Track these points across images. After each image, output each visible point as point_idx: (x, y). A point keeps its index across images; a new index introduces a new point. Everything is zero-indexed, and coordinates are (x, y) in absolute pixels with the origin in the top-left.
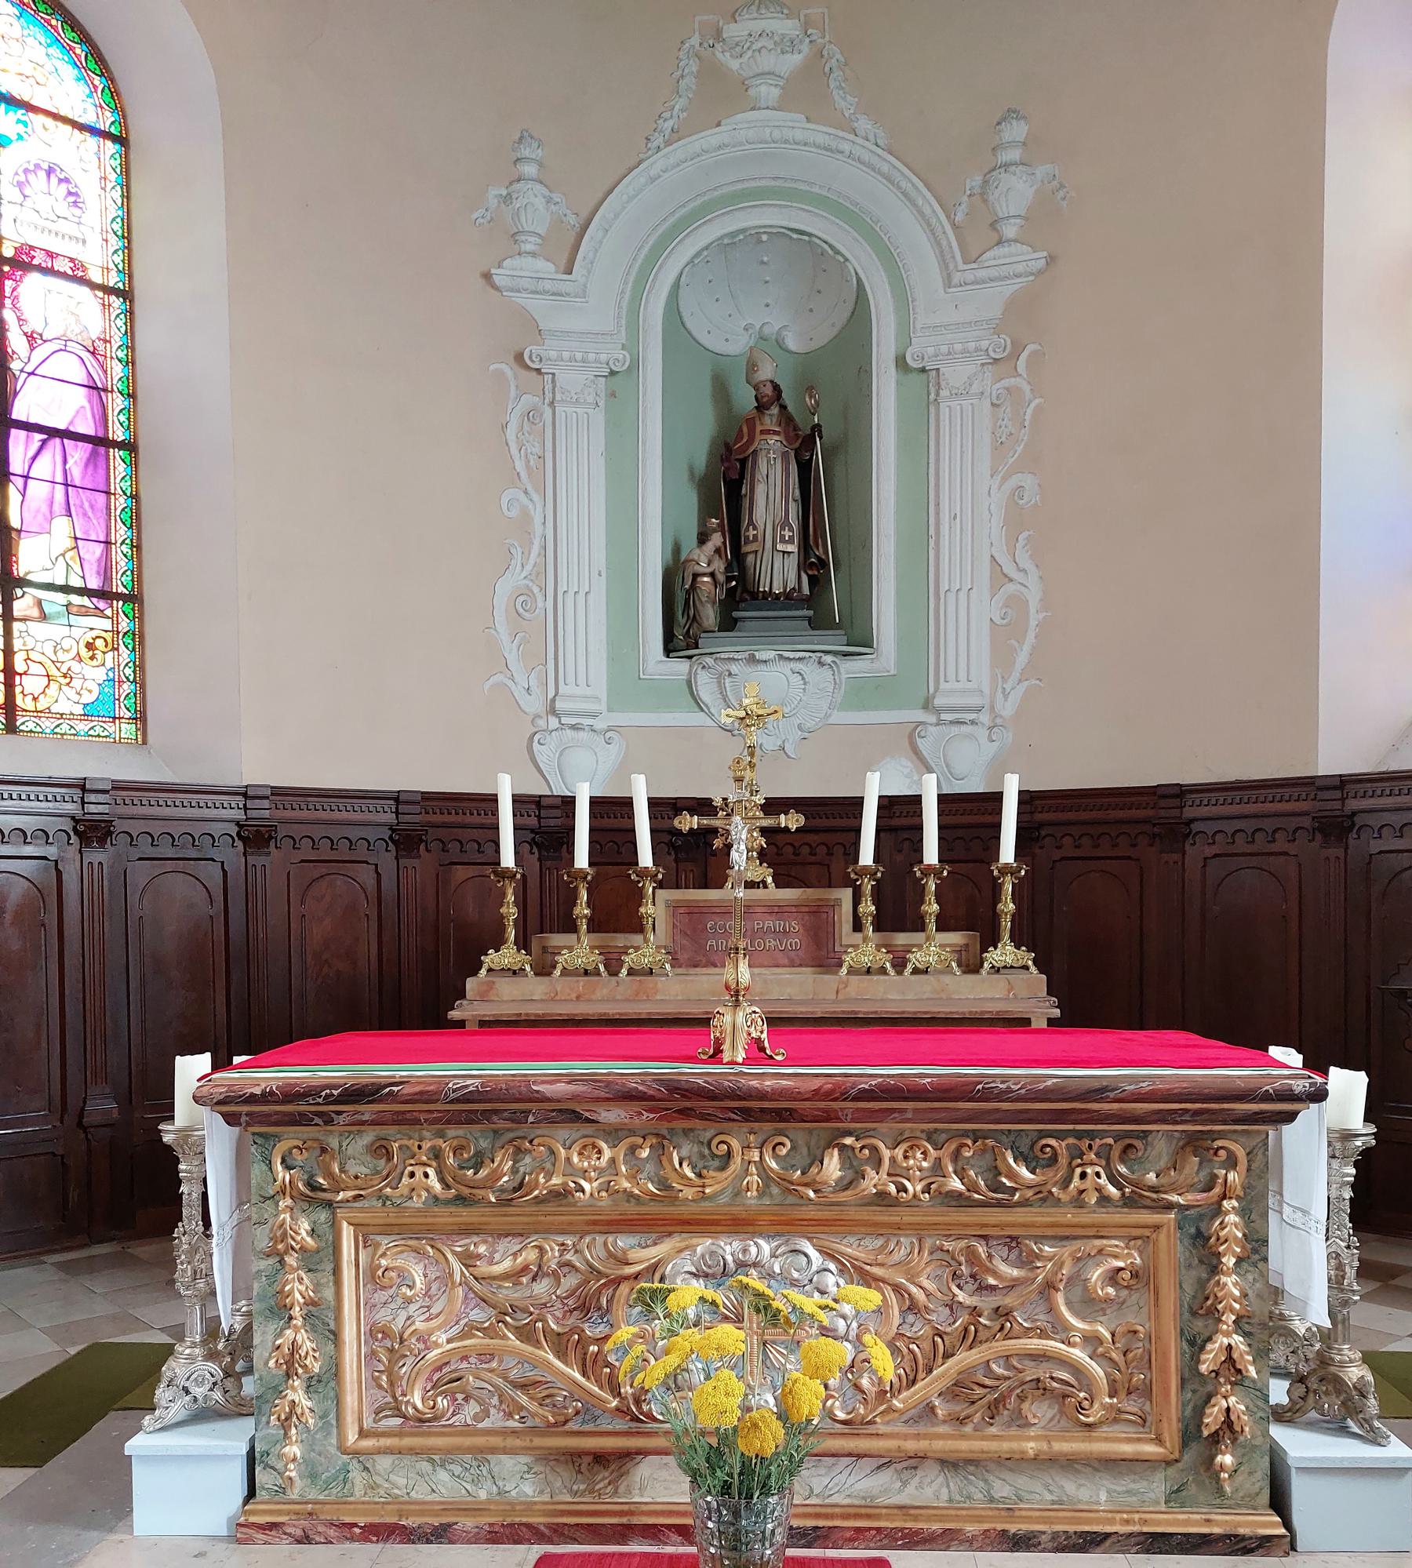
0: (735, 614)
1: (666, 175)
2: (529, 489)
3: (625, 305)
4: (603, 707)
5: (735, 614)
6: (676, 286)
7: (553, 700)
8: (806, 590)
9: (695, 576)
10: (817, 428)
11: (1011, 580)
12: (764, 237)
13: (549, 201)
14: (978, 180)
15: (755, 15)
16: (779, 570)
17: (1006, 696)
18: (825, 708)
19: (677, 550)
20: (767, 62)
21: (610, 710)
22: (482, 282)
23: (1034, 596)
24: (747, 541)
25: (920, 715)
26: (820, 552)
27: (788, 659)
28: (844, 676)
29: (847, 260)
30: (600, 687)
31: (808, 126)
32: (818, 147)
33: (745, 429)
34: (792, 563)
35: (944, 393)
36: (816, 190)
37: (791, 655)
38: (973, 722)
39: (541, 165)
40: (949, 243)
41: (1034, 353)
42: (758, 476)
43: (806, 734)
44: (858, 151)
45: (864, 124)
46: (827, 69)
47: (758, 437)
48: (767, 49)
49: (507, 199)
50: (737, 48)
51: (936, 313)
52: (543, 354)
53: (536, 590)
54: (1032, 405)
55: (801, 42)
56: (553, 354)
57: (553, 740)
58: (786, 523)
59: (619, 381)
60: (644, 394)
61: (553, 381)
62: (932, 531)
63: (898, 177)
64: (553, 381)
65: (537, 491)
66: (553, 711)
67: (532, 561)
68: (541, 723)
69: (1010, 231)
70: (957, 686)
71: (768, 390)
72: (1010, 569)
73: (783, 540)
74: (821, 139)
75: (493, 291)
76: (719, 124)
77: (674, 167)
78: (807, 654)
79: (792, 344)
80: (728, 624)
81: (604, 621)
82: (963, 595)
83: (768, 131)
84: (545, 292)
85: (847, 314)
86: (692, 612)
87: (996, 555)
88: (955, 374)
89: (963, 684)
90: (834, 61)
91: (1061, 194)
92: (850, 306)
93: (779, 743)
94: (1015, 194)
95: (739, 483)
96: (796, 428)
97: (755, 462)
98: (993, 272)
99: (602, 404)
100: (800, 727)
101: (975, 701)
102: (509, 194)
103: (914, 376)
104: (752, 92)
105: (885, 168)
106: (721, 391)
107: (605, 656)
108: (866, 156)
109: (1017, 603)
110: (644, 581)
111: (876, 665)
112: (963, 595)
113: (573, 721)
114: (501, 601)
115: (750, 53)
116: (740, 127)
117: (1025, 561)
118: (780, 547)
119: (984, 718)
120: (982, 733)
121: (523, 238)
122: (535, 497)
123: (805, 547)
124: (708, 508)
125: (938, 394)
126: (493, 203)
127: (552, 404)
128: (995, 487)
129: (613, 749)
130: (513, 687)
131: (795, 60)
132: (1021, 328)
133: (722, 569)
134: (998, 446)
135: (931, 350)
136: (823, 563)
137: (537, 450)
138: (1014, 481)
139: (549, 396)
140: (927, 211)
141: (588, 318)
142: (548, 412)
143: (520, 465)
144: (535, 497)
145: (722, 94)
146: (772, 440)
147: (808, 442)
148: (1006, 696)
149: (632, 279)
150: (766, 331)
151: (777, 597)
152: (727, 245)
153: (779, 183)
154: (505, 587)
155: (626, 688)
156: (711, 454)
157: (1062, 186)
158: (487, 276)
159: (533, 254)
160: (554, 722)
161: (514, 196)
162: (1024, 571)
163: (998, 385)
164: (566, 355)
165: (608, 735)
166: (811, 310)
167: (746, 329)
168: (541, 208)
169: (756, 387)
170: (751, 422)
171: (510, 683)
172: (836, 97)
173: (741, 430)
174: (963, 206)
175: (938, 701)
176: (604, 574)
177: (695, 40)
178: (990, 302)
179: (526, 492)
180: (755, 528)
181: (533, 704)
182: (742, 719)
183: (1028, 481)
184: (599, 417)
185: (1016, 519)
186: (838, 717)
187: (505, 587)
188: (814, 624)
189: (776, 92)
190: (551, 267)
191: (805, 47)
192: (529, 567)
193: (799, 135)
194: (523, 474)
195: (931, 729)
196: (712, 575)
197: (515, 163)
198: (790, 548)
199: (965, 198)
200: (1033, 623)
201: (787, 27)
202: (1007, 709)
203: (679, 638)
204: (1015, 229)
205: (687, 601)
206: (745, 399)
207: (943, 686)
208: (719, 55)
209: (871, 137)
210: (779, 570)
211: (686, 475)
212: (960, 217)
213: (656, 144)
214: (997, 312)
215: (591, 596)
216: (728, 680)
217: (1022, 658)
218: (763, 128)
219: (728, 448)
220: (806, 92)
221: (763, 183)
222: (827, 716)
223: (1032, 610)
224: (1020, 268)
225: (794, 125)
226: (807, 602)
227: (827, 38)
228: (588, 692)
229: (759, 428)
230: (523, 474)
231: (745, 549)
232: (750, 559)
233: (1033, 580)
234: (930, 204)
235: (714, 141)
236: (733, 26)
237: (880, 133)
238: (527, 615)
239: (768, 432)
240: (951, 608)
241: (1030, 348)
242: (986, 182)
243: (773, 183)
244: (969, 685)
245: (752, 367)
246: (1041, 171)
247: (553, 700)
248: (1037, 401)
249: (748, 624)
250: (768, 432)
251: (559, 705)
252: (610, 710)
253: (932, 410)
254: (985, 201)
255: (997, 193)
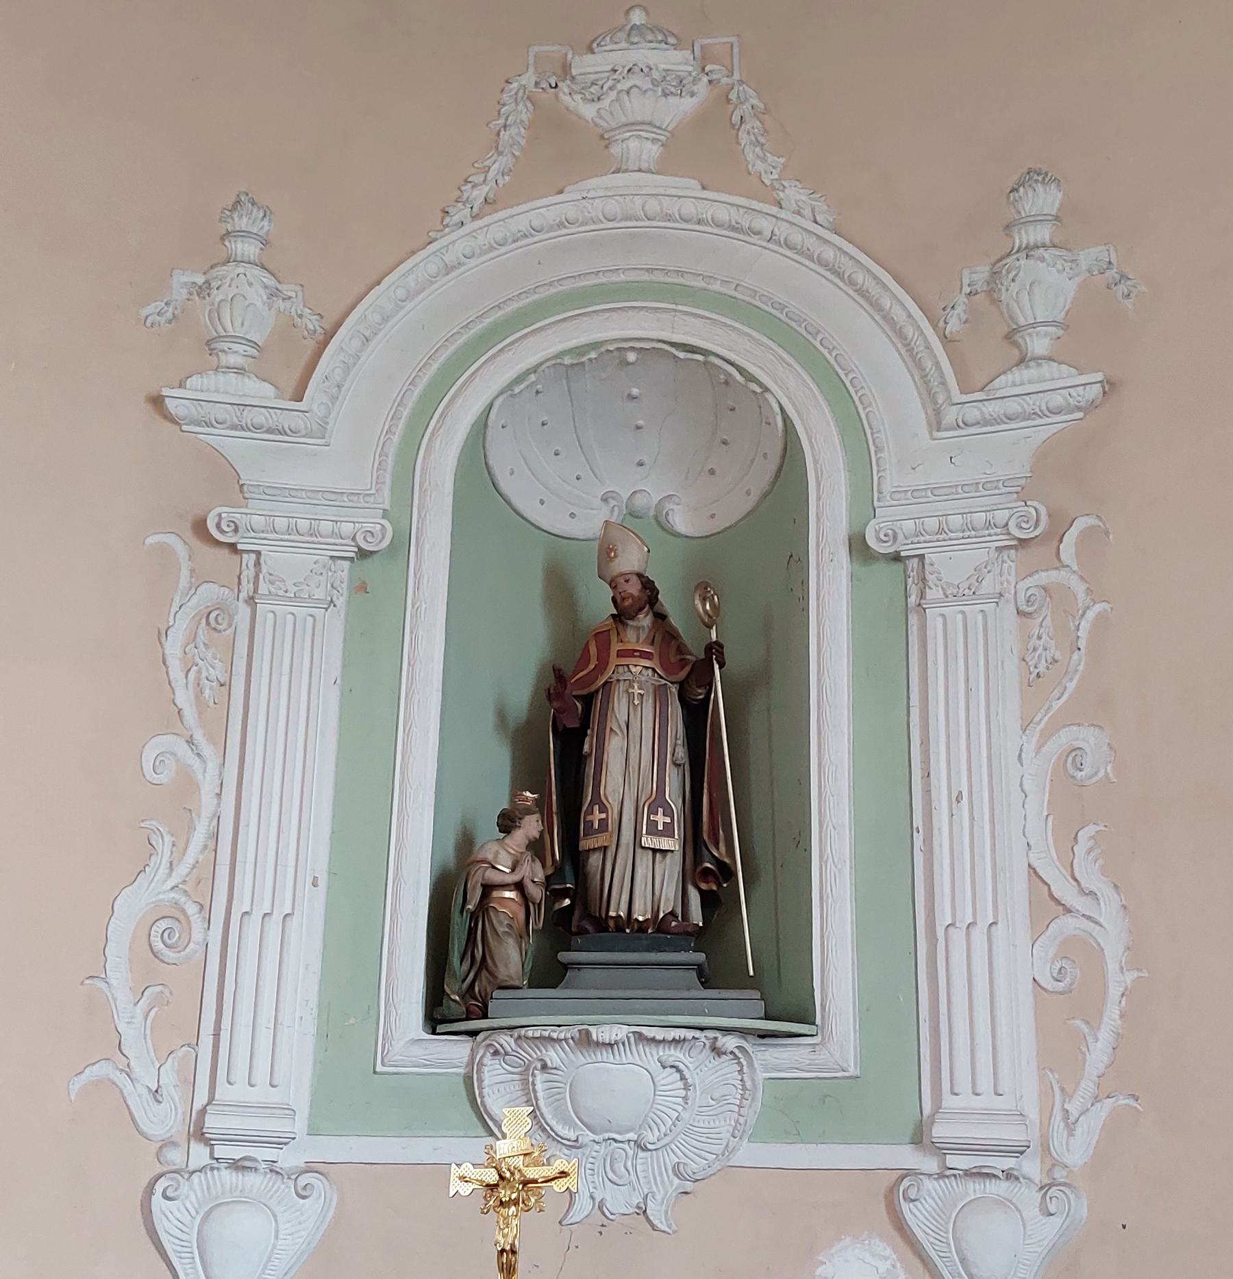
0: (564, 956)
1: (472, 262)
2: (199, 736)
3: (392, 451)
4: (300, 1126)
5: (564, 956)
6: (481, 427)
7: (203, 1112)
8: (697, 917)
9: (488, 888)
10: (715, 650)
11: (1068, 910)
12: (632, 357)
13: (274, 294)
14: (981, 274)
15: (624, 45)
16: (647, 878)
17: (1071, 1128)
18: (726, 1135)
19: (466, 843)
20: (641, 107)
21: (313, 1132)
22: (149, 408)
23: (1112, 938)
24: (590, 831)
25: (907, 1157)
26: (720, 852)
27: (653, 1040)
28: (761, 1075)
29: (767, 390)
30: (297, 1088)
31: (706, 194)
32: (719, 225)
33: (593, 650)
34: (671, 870)
35: (933, 594)
36: (717, 287)
37: (659, 1034)
38: (1009, 1175)
39: (265, 243)
40: (937, 364)
41: (1088, 532)
42: (611, 724)
43: (689, 1184)
44: (783, 231)
45: (794, 194)
46: (736, 119)
47: (614, 660)
48: (641, 86)
49: (204, 290)
50: (594, 91)
51: (913, 464)
52: (242, 520)
53: (192, 909)
54: (1090, 615)
55: (695, 81)
56: (258, 521)
57: (192, 1191)
58: (659, 802)
59: (373, 568)
60: (417, 588)
61: (257, 564)
62: (918, 821)
63: (848, 267)
64: (257, 564)
65: (211, 740)
66: (199, 1134)
67: (190, 858)
68: (175, 1157)
69: (1038, 345)
70: (977, 1103)
71: (634, 588)
72: (1064, 890)
73: (653, 830)
74: (723, 214)
75: (168, 424)
76: (561, 192)
77: (483, 253)
78: (690, 1034)
79: (681, 522)
80: (548, 974)
81: (316, 966)
82: (979, 935)
83: (638, 201)
84: (257, 428)
85: (768, 477)
86: (479, 954)
87: (1035, 865)
88: (950, 564)
89: (986, 1101)
90: (746, 107)
91: (1122, 288)
92: (773, 465)
93: (636, 1199)
94: (1045, 290)
95: (581, 733)
96: (681, 649)
97: (607, 700)
98: (1013, 406)
99: (340, 602)
100: (677, 1172)
101: (1012, 1134)
102: (207, 282)
103: (882, 567)
104: (616, 150)
105: (829, 254)
106: (559, 590)
107: (312, 1029)
108: (797, 238)
109: (1081, 953)
110: (396, 894)
111: (822, 1057)
112: (979, 935)
113: (237, 1152)
114: (122, 930)
115: (613, 94)
116: (597, 195)
117: (1092, 878)
118: (647, 841)
119: (1031, 1167)
120: (1029, 1198)
121: (225, 346)
122: (207, 750)
123: (695, 842)
124: (527, 772)
125: (922, 595)
126: (179, 293)
127: (251, 601)
128: (1029, 749)
129: (312, 1206)
130: (128, 1088)
131: (687, 105)
132: (1057, 508)
133: (540, 876)
134: (1033, 682)
135: (909, 526)
136: (726, 872)
137: (218, 672)
138: (1064, 738)
139: (247, 587)
140: (899, 315)
141: (326, 468)
142: (244, 611)
143: (184, 698)
144: (207, 750)
145: (566, 149)
146: (638, 667)
147: (700, 673)
148: (1071, 1128)
149: (406, 413)
150: (640, 502)
151: (642, 927)
152: (570, 368)
153: (660, 277)
154: (133, 905)
155: (349, 1086)
156: (536, 692)
157: (1124, 277)
158: (157, 401)
159: (240, 371)
160: (200, 1155)
161: (214, 284)
162: (1092, 893)
163: (1029, 582)
164: (281, 523)
165: (303, 1180)
166: (712, 472)
167: (605, 500)
168: (259, 303)
169: (613, 584)
170: (602, 638)
171: (122, 1079)
172: (750, 157)
173: (586, 650)
174: (959, 310)
175: (941, 1131)
176: (322, 882)
177: (529, 79)
178: (1010, 452)
179: (190, 742)
180: (603, 809)
181: (162, 1120)
182: (492, 1187)
183: (1089, 739)
184: (335, 624)
185: (1071, 802)
186: (749, 1153)
187: (133, 905)
188: (707, 979)
189: (655, 150)
190: (269, 390)
191: (702, 87)
192: (182, 870)
193: (689, 208)
194: (190, 713)
195: (929, 1184)
196: (519, 886)
197: (222, 239)
198: (665, 843)
199: (963, 298)
200: (1114, 991)
201: (675, 60)
202: (1076, 1151)
203: (456, 995)
204: (1047, 341)
205: (472, 932)
206: (598, 603)
207: (949, 1101)
208: (566, 99)
209: (807, 212)
210: (647, 878)
211: (490, 718)
212: (953, 326)
213: (456, 219)
214: (1020, 468)
215: (294, 923)
216: (540, 1078)
217: (1098, 1054)
218: (634, 197)
219: (560, 676)
220: (702, 148)
221: (632, 276)
222: (728, 1150)
223: (1112, 967)
224: (1058, 399)
225: (684, 194)
226: (698, 937)
227: (737, 76)
228: (274, 1096)
229: (616, 647)
230: (190, 713)
231: (585, 844)
232: (595, 860)
233: (1109, 910)
234: (904, 307)
235: (552, 215)
236: (589, 58)
237: (821, 206)
238: (170, 955)
239: (630, 653)
240: (958, 956)
241: (1081, 524)
242: (995, 274)
243: (646, 277)
244: (998, 1103)
245: (607, 552)
246: (1088, 256)
247: (203, 1112)
248: (1098, 607)
249: (587, 974)
250: (630, 653)
251: (211, 1122)
252: (313, 1132)
253: (913, 620)
254: (996, 302)
255: (1014, 287)
